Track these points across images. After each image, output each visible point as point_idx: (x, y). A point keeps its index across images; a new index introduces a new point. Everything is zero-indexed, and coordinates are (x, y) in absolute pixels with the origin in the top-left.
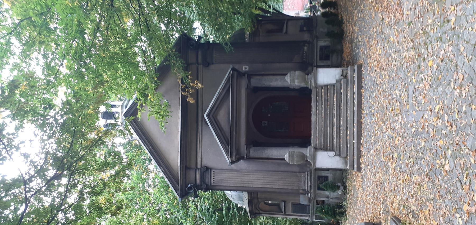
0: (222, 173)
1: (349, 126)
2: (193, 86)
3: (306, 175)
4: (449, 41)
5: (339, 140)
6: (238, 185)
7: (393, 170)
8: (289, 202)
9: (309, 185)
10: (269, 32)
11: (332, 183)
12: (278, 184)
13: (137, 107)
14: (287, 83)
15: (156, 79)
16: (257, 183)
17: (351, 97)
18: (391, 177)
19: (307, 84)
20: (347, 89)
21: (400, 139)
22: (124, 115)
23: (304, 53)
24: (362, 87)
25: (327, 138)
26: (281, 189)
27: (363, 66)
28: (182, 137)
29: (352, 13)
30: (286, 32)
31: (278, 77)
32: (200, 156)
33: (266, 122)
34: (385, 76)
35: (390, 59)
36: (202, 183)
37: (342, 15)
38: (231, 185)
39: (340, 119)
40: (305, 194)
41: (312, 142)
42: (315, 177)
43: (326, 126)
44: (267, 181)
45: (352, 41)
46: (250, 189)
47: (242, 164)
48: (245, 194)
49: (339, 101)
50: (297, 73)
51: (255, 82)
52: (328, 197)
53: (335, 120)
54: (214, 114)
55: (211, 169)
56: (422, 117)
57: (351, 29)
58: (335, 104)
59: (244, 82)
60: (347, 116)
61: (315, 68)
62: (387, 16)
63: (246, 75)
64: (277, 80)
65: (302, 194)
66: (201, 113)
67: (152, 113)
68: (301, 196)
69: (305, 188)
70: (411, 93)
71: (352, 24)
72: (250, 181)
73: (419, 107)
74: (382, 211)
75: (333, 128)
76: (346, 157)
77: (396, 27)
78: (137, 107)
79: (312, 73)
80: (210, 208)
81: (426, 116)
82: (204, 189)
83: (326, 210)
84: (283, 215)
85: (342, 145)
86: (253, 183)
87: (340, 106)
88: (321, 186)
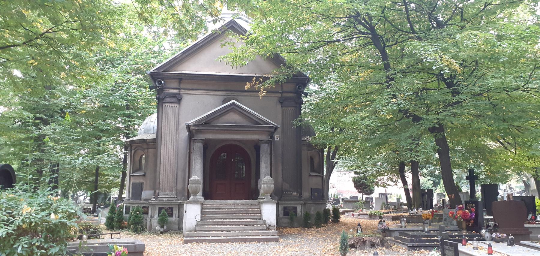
0: (175, 115)
1: (225, 232)
3: (174, 196)
8: (144, 180)
9: (164, 199)
10: (312, 159)
11: (167, 221)
12: (164, 169)
14: (263, 177)
15: (268, 55)
16: (165, 148)
20: (257, 230)
24: (259, 242)
27: (278, 243)
28: (211, 76)
29: (324, 234)
30: (310, 175)
31: (269, 169)
32: (191, 93)
33: (226, 157)
36: (166, 95)
38: (163, 123)
39: (230, 225)
41: (208, 201)
43: (223, 213)
44: (167, 159)
45: (299, 234)
46: (159, 141)
47: (185, 134)
48: (153, 136)
49: (246, 224)
50: (272, 186)
51: (265, 149)
52: (152, 217)
53: (230, 220)
54: (235, 109)
55: (179, 104)
58: (244, 220)
59: (264, 137)
60: (233, 230)
61: (276, 202)
63: (271, 139)
64: (266, 168)
65: (155, 192)
66: (235, 95)
68: (152, 192)
72: (168, 143)
79: (272, 199)
82: (159, 97)
84: (130, 173)
86: (166, 145)
87: (242, 225)
88: (164, 210)
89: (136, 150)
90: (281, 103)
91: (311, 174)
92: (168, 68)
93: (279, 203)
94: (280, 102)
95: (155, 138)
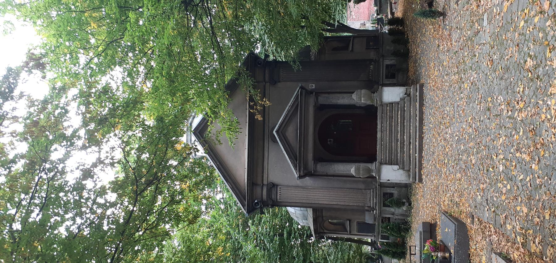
0: (288, 190)
1: (411, 141)
2: (261, 103)
3: (372, 192)
4: (475, 70)
5: (403, 155)
6: (304, 201)
7: (445, 174)
10: (335, 49)
13: (208, 124)
14: (354, 101)
17: (413, 114)
18: (443, 180)
19: (373, 102)
21: (449, 147)
23: (371, 71)
24: (424, 104)
25: (392, 154)
27: (425, 85)
30: (352, 50)
31: (345, 95)
34: (440, 95)
35: (444, 80)
37: (407, 34)
39: (404, 135)
42: (380, 194)
43: (390, 142)
44: (333, 198)
45: (416, 62)
47: (308, 181)
48: (310, 212)
49: (403, 118)
50: (363, 91)
51: (323, 100)
52: (393, 214)
53: (399, 136)
54: (283, 129)
55: (277, 186)
56: (462, 127)
57: (415, 49)
59: (312, 101)
60: (410, 132)
62: (442, 43)
63: (314, 93)
64: (343, 98)
67: (225, 129)
68: (367, 213)
70: (456, 108)
71: (416, 44)
72: (316, 197)
73: (460, 119)
74: (437, 212)
75: (397, 144)
76: (409, 171)
77: (448, 54)
78: (208, 124)
80: (270, 231)
81: (464, 126)
83: (391, 226)
85: (405, 159)
86: (319, 199)
87: (404, 122)
89: (324, 228)
91: (351, 49)
94: (275, 83)
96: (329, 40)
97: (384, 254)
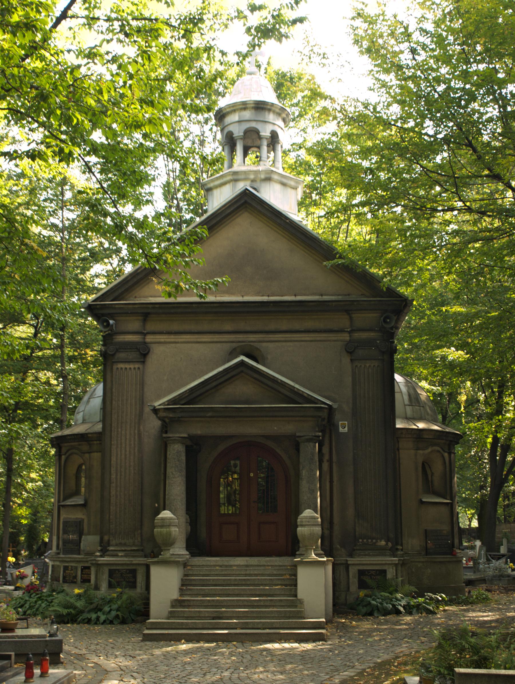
10: (425, 466)
16: (119, 453)
22: (247, 189)
23: (374, 541)
26: (110, 500)
38: (114, 402)
40: (101, 546)
48: (99, 427)
55: (144, 362)
68: (97, 538)
69: (112, 546)
72: (123, 441)
89: (70, 455)
90: (350, 353)
92: (122, 293)
93: (349, 562)
94: (348, 352)
95: (101, 430)
96: (446, 455)
97: (159, 514)
